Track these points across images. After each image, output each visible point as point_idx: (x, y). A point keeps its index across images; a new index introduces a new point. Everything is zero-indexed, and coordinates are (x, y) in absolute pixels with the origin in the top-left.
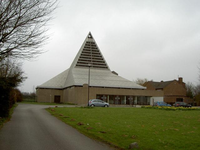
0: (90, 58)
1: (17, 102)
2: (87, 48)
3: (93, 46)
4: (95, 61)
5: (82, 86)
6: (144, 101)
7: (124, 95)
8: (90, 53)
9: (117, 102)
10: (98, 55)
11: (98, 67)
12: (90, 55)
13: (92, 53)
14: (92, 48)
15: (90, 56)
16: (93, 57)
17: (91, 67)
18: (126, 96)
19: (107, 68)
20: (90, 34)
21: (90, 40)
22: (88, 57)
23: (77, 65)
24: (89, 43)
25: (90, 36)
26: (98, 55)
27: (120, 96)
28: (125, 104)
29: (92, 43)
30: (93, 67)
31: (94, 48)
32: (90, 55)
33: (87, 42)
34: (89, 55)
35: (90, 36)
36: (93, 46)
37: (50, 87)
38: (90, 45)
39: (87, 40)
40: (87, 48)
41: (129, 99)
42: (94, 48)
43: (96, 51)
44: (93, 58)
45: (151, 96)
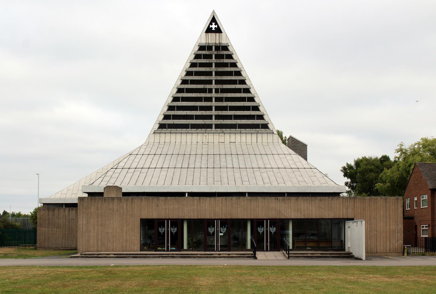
0: (209, 99)
1: (344, 250)
2: (202, 65)
3: (222, 57)
4: (203, 108)
5: (101, 194)
6: (89, 229)
7: (246, 217)
8: (210, 82)
9: (168, 240)
10: (238, 86)
11: (186, 126)
12: (213, 91)
13: (217, 82)
14: (217, 65)
15: (210, 91)
16: (219, 95)
17: (212, 128)
18: (252, 220)
19: (265, 126)
20: (214, 20)
21: (213, 39)
22: (203, 95)
23: (162, 126)
24: (209, 48)
25: (214, 26)
26: (238, 86)
27: (274, 222)
28: (291, 247)
29: (218, 48)
30: (218, 126)
31: (226, 65)
32: (213, 91)
33: (202, 48)
34: (203, 91)
35: (214, 26)
36: (222, 57)
37: (60, 199)
38: (210, 57)
39: (203, 42)
40: (202, 65)
41: (260, 230)
42: (226, 65)
43: (230, 73)
44: (218, 99)
45: (350, 216)
